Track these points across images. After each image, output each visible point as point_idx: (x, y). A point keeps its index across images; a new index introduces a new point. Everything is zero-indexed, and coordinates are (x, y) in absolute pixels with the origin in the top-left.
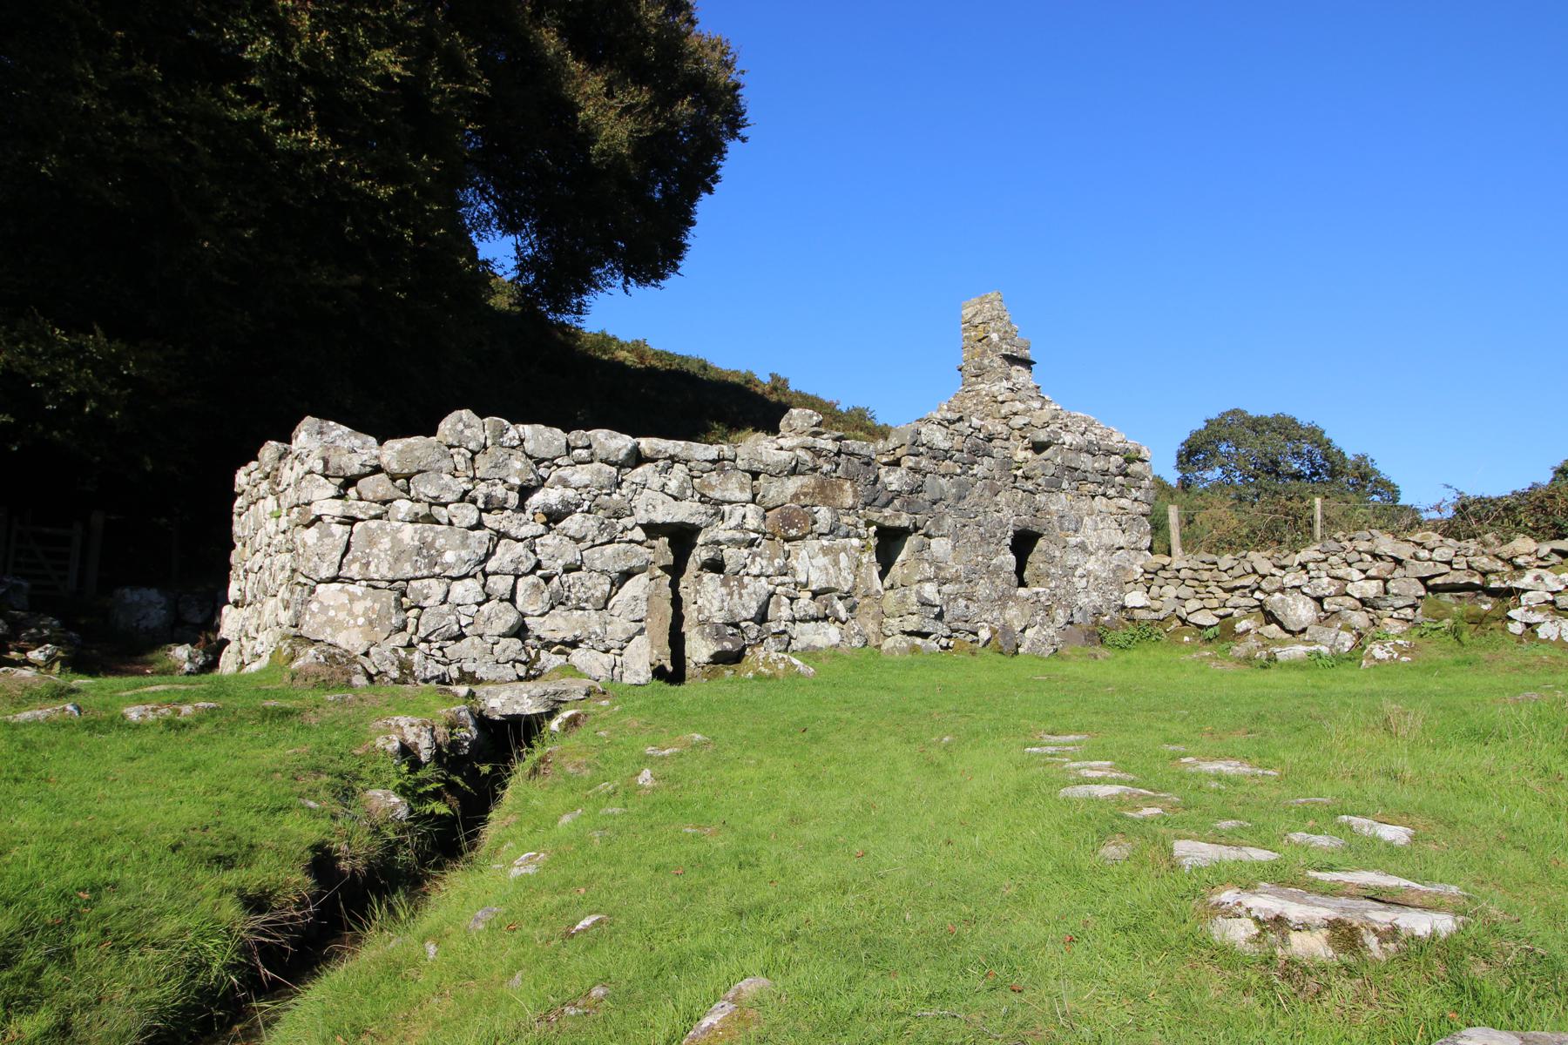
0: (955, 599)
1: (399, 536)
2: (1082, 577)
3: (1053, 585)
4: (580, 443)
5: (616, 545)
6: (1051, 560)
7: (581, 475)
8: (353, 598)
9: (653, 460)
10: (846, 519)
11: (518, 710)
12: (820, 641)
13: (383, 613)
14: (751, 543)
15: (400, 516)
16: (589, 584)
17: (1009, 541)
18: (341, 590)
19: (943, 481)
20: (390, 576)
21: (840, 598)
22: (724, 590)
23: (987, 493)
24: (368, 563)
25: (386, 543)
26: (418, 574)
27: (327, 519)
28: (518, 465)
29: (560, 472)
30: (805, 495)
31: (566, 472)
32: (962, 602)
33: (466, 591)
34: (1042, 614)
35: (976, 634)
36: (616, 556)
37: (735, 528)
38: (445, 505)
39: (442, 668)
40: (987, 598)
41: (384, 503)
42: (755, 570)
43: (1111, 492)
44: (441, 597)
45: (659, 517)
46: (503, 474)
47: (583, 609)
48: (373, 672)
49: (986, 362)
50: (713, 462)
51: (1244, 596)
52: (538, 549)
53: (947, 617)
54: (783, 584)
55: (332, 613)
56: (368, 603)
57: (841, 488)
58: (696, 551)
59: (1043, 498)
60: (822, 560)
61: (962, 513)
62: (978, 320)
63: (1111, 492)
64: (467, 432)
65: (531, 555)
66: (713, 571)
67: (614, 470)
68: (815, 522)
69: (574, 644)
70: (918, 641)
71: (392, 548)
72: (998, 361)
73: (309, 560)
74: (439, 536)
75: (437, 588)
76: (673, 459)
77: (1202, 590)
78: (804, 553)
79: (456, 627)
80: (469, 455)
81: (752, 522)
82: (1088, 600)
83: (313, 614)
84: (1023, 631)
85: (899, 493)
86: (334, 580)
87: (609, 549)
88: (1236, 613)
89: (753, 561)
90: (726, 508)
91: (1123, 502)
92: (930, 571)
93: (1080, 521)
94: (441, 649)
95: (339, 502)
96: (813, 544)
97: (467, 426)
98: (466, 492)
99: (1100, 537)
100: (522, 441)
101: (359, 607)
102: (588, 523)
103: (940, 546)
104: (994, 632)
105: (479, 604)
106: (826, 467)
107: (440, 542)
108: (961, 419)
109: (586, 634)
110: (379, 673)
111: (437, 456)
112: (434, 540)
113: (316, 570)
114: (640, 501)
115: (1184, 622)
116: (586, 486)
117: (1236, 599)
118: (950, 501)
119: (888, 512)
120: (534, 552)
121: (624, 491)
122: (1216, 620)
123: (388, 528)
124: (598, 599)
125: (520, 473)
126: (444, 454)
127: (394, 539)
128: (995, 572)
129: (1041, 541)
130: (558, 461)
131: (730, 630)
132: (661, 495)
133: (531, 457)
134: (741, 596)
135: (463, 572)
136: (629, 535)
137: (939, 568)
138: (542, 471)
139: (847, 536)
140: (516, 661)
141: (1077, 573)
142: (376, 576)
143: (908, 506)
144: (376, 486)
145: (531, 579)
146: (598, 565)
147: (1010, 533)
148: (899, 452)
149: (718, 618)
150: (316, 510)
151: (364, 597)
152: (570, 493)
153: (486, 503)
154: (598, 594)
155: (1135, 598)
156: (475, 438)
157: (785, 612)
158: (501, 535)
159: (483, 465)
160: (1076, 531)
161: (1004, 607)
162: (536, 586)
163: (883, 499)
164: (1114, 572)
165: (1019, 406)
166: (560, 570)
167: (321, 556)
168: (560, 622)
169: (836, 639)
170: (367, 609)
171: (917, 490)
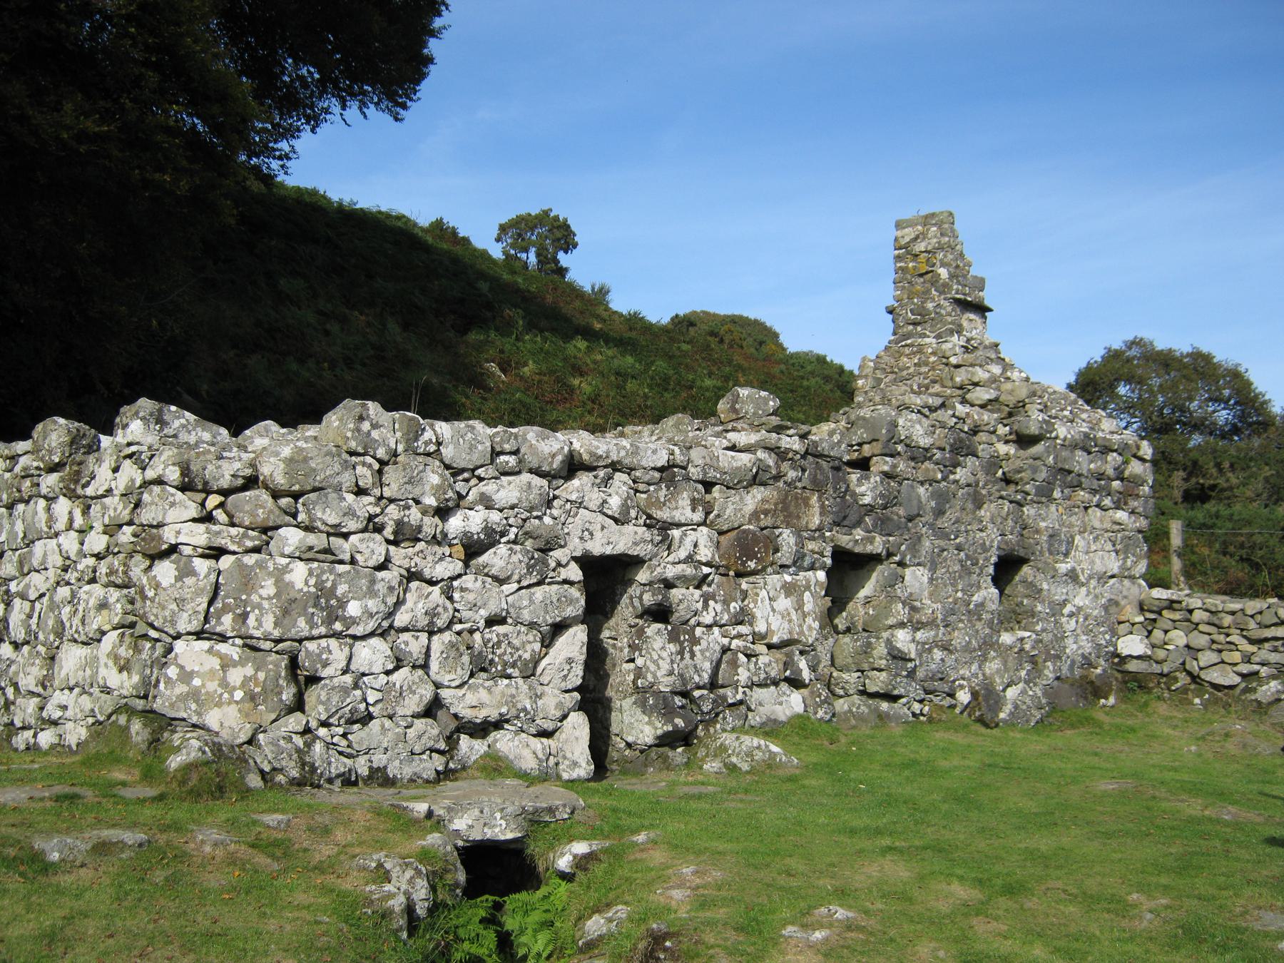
0: (930, 650)
1: (287, 577)
2: (1071, 615)
3: (1038, 628)
4: (507, 447)
5: (546, 588)
6: (1036, 593)
7: (508, 491)
8: (226, 664)
9: (590, 468)
10: (811, 546)
11: (489, 834)
12: (782, 713)
13: (270, 685)
14: (702, 581)
15: (287, 550)
16: (516, 642)
17: (991, 570)
18: (210, 651)
19: (921, 490)
20: (276, 634)
21: (802, 653)
22: (672, 648)
23: (970, 506)
24: (245, 616)
25: (269, 588)
26: (315, 632)
27: (187, 550)
28: (435, 479)
29: (483, 488)
30: (766, 513)
31: (489, 488)
32: (938, 654)
33: (372, 654)
34: (1028, 666)
35: (952, 695)
36: (546, 605)
37: (685, 562)
38: (346, 536)
39: (348, 762)
40: (967, 648)
41: (265, 530)
42: (707, 618)
43: (1107, 502)
44: (343, 664)
45: (597, 547)
46: (417, 492)
47: (509, 677)
48: (267, 769)
49: (930, 306)
50: (661, 470)
51: (1275, 650)
52: (456, 596)
53: (920, 674)
54: (739, 636)
55: (197, 682)
56: (249, 670)
57: (807, 505)
58: (634, 590)
59: (1032, 512)
60: (784, 603)
61: (942, 534)
62: (920, 247)
63: (1107, 502)
64: (375, 434)
65: (448, 603)
66: (656, 620)
67: (544, 482)
68: (777, 550)
69: (498, 725)
70: (885, 706)
71: (277, 595)
72: (948, 306)
73: (164, 608)
74: (341, 581)
75: (338, 653)
76: (615, 467)
77: (1221, 638)
78: (763, 593)
79: (363, 706)
80: (376, 466)
81: (705, 553)
82: (1077, 646)
83: (169, 681)
84: (1004, 690)
85: (870, 509)
86: (199, 635)
87: (539, 592)
88: (1264, 671)
89: (706, 606)
90: (676, 533)
91: (1121, 515)
92: (900, 611)
93: (1070, 542)
94: (344, 735)
95: (202, 527)
96: (774, 580)
97: (375, 426)
98: (371, 518)
99: (1093, 562)
100: (439, 444)
101: (235, 676)
102: (515, 558)
103: (916, 578)
104: (975, 695)
105: (388, 673)
106: (792, 474)
107: (341, 589)
108: (943, 405)
109: (513, 712)
110: (274, 769)
111: (337, 467)
112: (334, 586)
113: (173, 623)
114: (574, 527)
115: (1195, 678)
116: (512, 507)
117: (1264, 653)
118: (928, 518)
119: (859, 534)
120: (450, 598)
121: (555, 512)
122: (1237, 679)
123: (271, 565)
124: (526, 663)
125: (438, 490)
126: (346, 466)
127: (279, 582)
128: (976, 613)
129: (1026, 570)
130: (480, 472)
131: (678, 701)
132: (600, 518)
133: (447, 467)
134: (693, 655)
135: (369, 628)
136: (564, 574)
137: (914, 609)
138: (461, 487)
139: (812, 568)
140: (432, 750)
141: (1066, 611)
142: (257, 634)
143: (884, 526)
144: (257, 504)
145: (447, 636)
146: (526, 616)
147: (994, 559)
148: (867, 451)
149: (665, 684)
150: (169, 536)
151: (242, 662)
152: (495, 516)
153: (395, 533)
154: (527, 656)
155: (1132, 645)
156: (384, 443)
157: (743, 675)
158: (413, 575)
159: (394, 483)
160: (1066, 555)
161: (984, 658)
162: (452, 645)
163: (853, 517)
164: (1106, 608)
165: (981, 374)
166: (482, 624)
167: (180, 602)
168: (483, 695)
169: (799, 709)
170: (246, 680)
171: (890, 502)
